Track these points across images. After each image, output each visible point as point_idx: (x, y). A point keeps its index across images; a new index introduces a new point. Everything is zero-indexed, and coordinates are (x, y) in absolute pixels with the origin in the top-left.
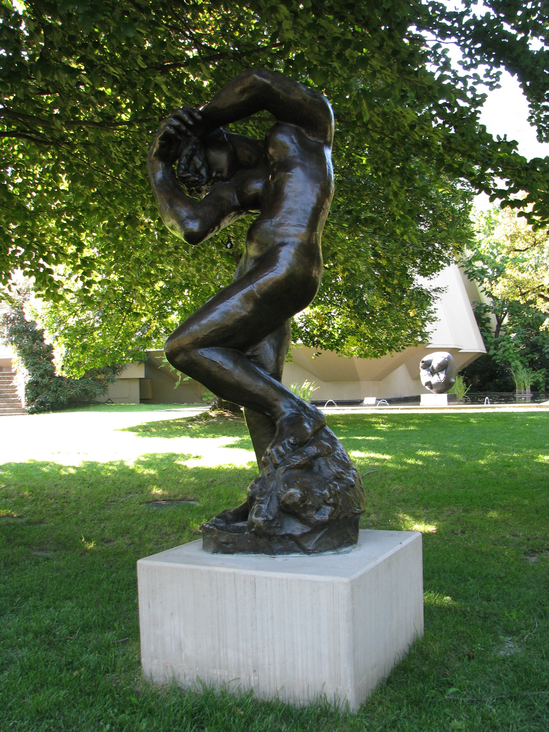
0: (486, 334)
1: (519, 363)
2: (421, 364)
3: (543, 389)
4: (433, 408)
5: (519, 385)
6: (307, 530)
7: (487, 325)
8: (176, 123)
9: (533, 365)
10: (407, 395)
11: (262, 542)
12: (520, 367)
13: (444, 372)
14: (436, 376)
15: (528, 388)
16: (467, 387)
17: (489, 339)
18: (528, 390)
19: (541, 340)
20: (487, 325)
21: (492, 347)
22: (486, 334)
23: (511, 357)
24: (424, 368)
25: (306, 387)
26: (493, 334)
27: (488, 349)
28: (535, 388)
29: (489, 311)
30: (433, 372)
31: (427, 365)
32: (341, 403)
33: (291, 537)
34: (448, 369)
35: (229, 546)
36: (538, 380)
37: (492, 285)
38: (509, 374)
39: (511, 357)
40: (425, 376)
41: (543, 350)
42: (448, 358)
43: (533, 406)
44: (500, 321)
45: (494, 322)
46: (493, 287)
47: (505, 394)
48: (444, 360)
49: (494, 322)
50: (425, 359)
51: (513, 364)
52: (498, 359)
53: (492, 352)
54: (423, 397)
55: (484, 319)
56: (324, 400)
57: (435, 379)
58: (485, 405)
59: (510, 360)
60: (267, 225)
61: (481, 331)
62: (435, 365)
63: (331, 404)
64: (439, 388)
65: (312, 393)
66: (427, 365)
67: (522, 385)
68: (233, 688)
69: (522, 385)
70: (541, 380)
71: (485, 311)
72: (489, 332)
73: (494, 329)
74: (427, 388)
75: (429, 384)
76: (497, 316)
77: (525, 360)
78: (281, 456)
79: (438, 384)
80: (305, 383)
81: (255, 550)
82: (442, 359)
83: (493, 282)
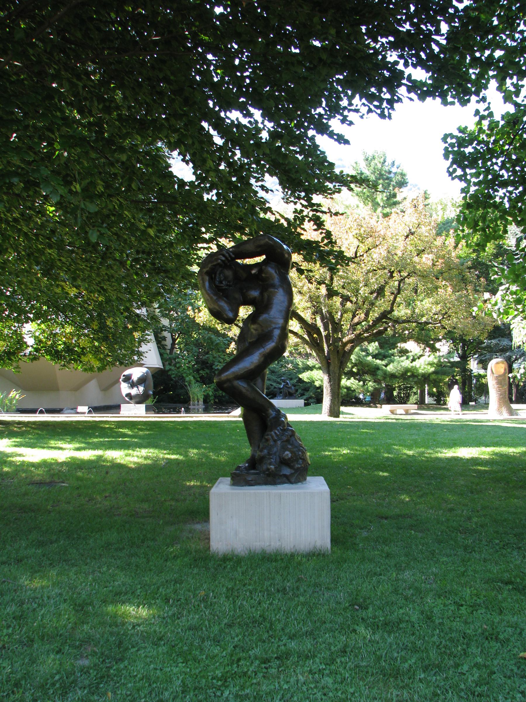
0: (163, 351)
1: (192, 378)
2: (122, 377)
3: (212, 402)
4: (129, 417)
5: (193, 398)
6: (293, 471)
7: (163, 343)
8: (223, 259)
9: (204, 380)
10: (103, 404)
11: (269, 479)
12: (193, 381)
13: (143, 385)
14: (135, 389)
15: (202, 400)
16: (154, 398)
17: (165, 356)
18: (201, 402)
19: (211, 358)
20: (163, 343)
21: (167, 363)
22: (163, 351)
23: (185, 373)
24: (124, 381)
25: (14, 396)
26: (168, 351)
27: (164, 365)
28: (206, 400)
29: (165, 330)
30: (133, 385)
31: (128, 379)
32: (50, 411)
33: (285, 476)
34: (147, 382)
35: (252, 482)
36: (208, 394)
37: (195, 313)
38: (183, 387)
39: (185, 373)
40: (125, 389)
41: (214, 367)
42: (147, 373)
43: (155, 417)
44: (174, 340)
45: (168, 342)
46: (196, 315)
47: (174, 405)
48: (143, 375)
49: (168, 342)
50: (126, 373)
51: (187, 379)
52: (173, 373)
53: (167, 368)
54: (122, 406)
55: (161, 338)
56: (36, 407)
57: (134, 391)
58: (182, 415)
59: (184, 375)
60: (264, 316)
61: (159, 348)
62: (135, 378)
63: (41, 412)
64: (137, 400)
65: (18, 400)
66: (128, 379)
67: (196, 398)
68: (268, 550)
69: (196, 398)
70: (211, 393)
71: (162, 330)
72: (165, 349)
73: (169, 347)
74: (127, 399)
75: (129, 395)
76: (172, 336)
77: (197, 376)
78: (277, 435)
79: (137, 396)
80: (12, 393)
81: (266, 483)
82: (141, 374)
83: (196, 311)
